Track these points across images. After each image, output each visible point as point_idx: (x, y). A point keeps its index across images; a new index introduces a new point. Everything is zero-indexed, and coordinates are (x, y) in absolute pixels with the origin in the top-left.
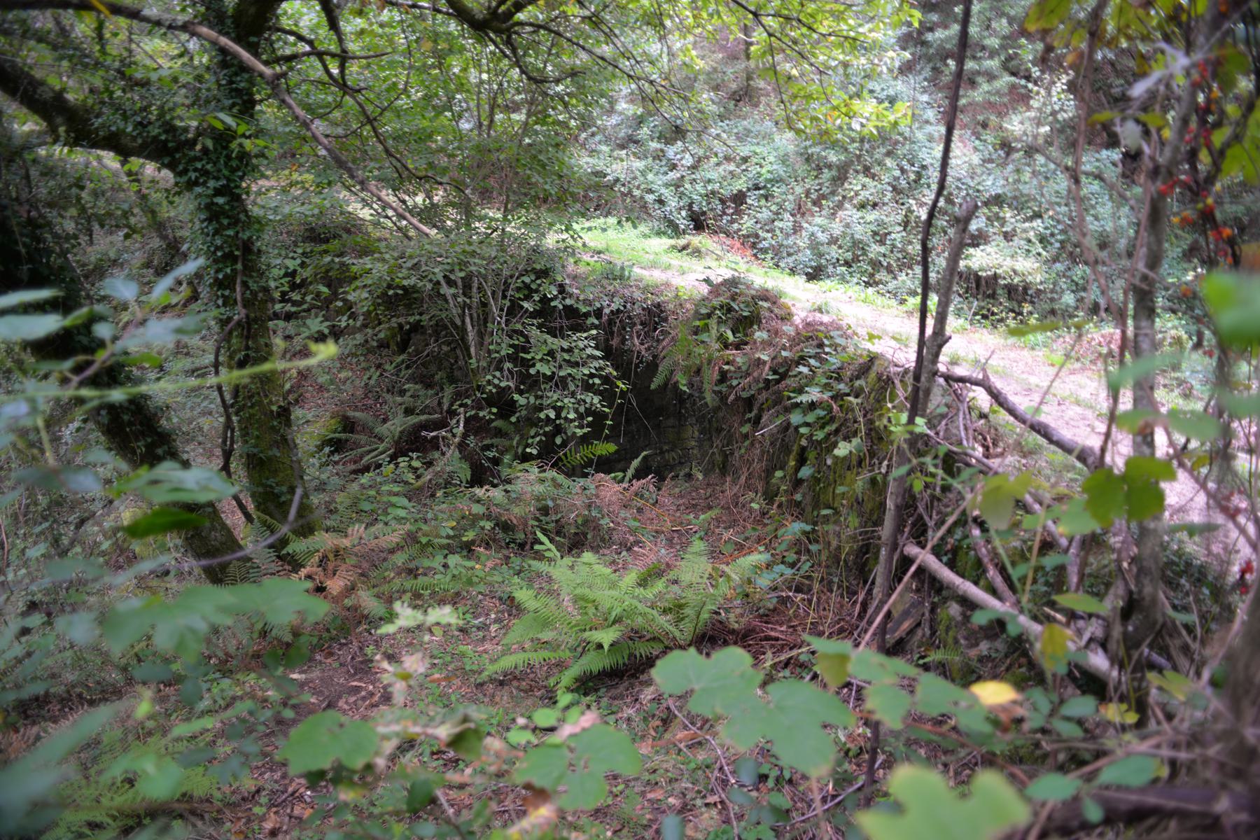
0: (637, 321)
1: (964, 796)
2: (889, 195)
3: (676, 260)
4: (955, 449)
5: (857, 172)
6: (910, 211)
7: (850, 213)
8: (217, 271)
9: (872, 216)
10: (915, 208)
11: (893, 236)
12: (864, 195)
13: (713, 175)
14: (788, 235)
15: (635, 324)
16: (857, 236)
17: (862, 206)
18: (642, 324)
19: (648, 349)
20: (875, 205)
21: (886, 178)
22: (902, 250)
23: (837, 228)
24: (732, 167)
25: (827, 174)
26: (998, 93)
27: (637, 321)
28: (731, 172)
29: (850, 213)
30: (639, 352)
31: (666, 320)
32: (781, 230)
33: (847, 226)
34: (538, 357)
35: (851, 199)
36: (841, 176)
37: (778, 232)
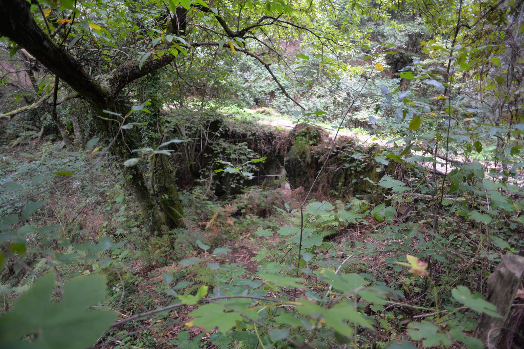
0: (262, 139)
1: (187, 229)
2: (329, 93)
3: (260, 116)
4: (416, 198)
5: (317, 85)
6: (335, 98)
7: (315, 99)
8: (151, 120)
9: (323, 100)
10: (337, 97)
11: (331, 107)
12: (320, 93)
13: (263, 84)
14: (291, 107)
15: (261, 140)
16: (319, 108)
17: (319, 97)
18: (264, 139)
19: (268, 148)
20: (323, 96)
21: (327, 87)
22: (334, 113)
23: (311, 104)
24: (268, 81)
25: (305, 85)
26: (360, 58)
27: (262, 139)
28: (268, 84)
29: (315, 99)
30: (264, 150)
31: (275, 137)
32: (289, 105)
33: (314, 104)
34: (232, 152)
35: (315, 94)
36: (310, 86)
37: (288, 106)
